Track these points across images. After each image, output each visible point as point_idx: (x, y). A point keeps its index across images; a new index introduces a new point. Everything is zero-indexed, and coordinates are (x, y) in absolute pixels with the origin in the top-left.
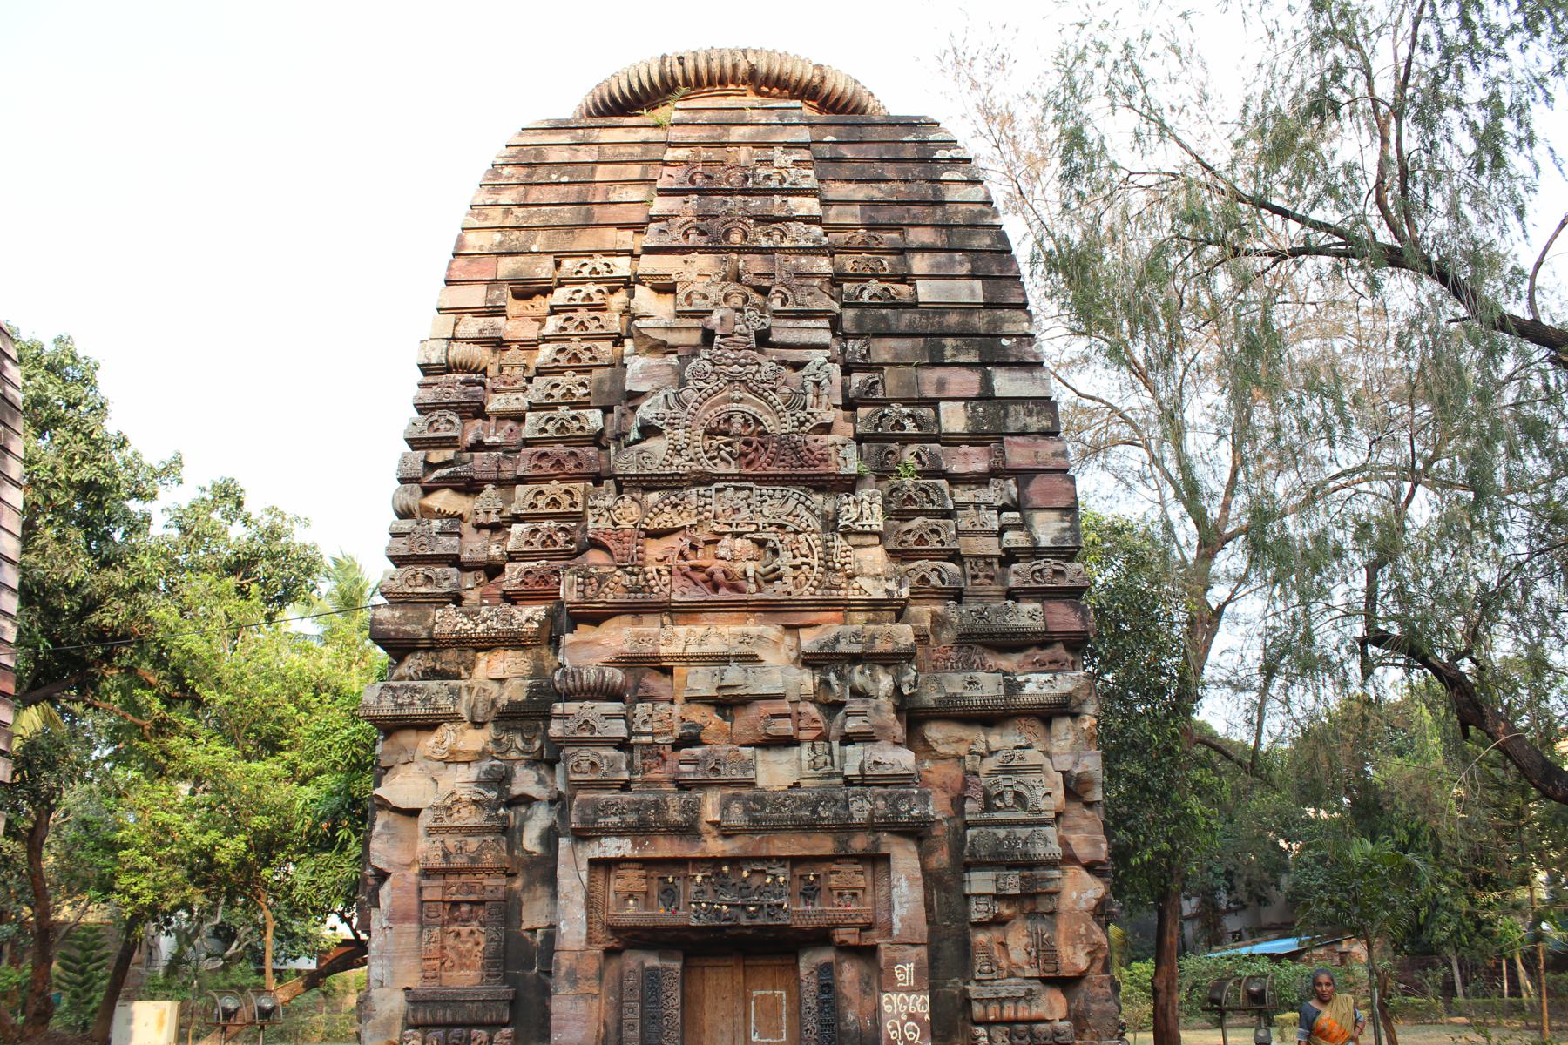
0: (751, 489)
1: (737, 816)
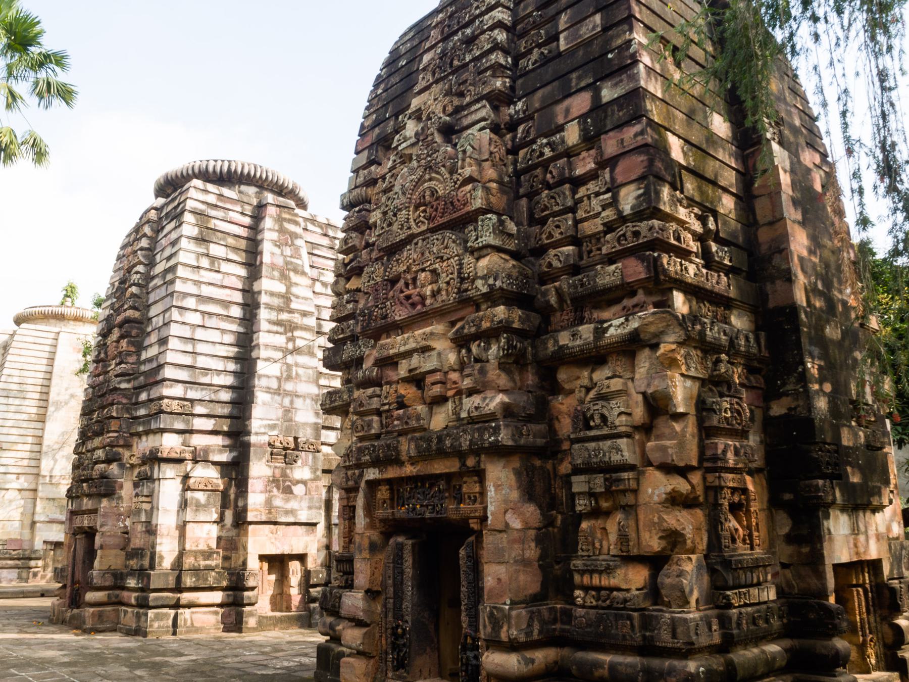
0: (428, 238)
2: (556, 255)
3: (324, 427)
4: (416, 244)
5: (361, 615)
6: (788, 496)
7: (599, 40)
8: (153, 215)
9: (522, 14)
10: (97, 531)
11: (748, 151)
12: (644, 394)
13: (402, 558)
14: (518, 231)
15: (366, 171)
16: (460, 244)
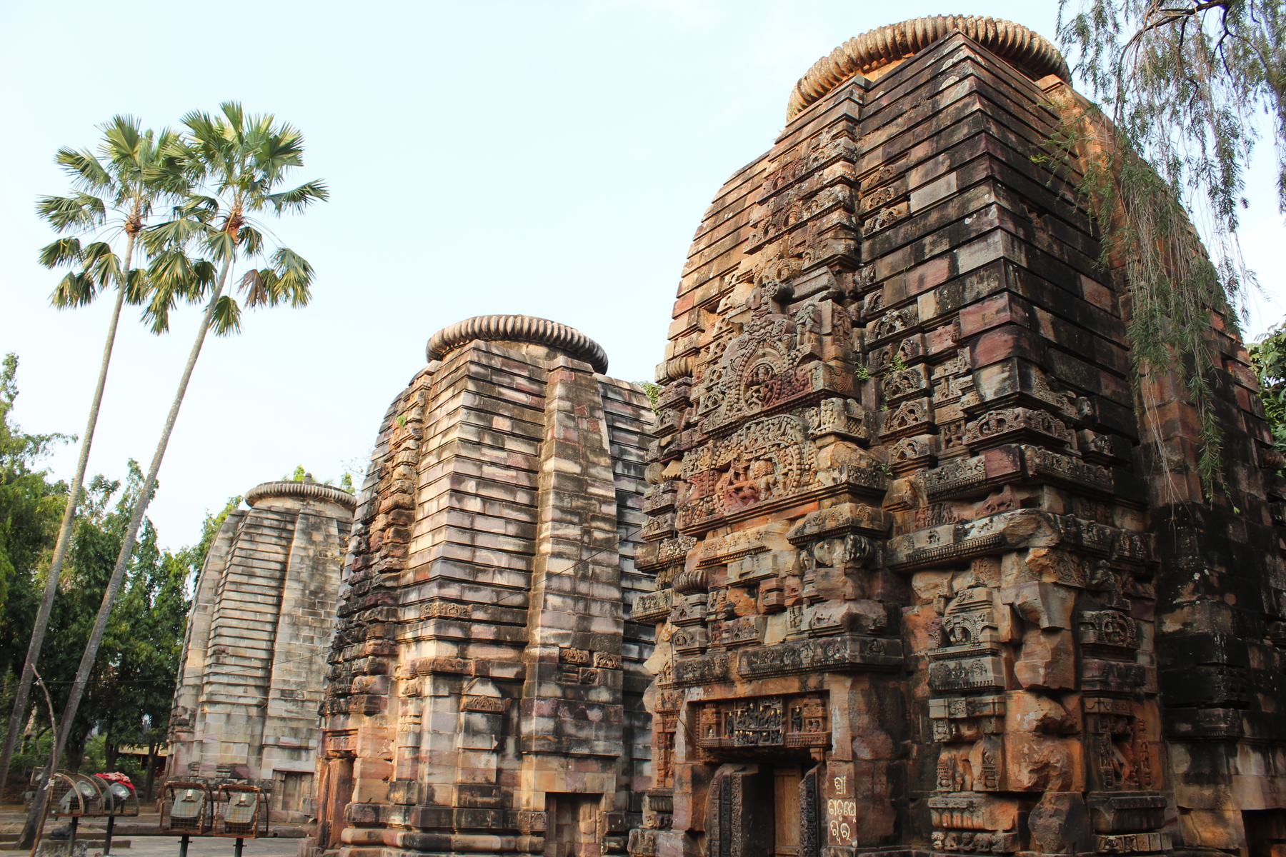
0: (762, 422)
1: (745, 670)
4: (749, 428)
6: (1185, 727)
8: (426, 380)
10: (356, 756)
12: (1011, 605)
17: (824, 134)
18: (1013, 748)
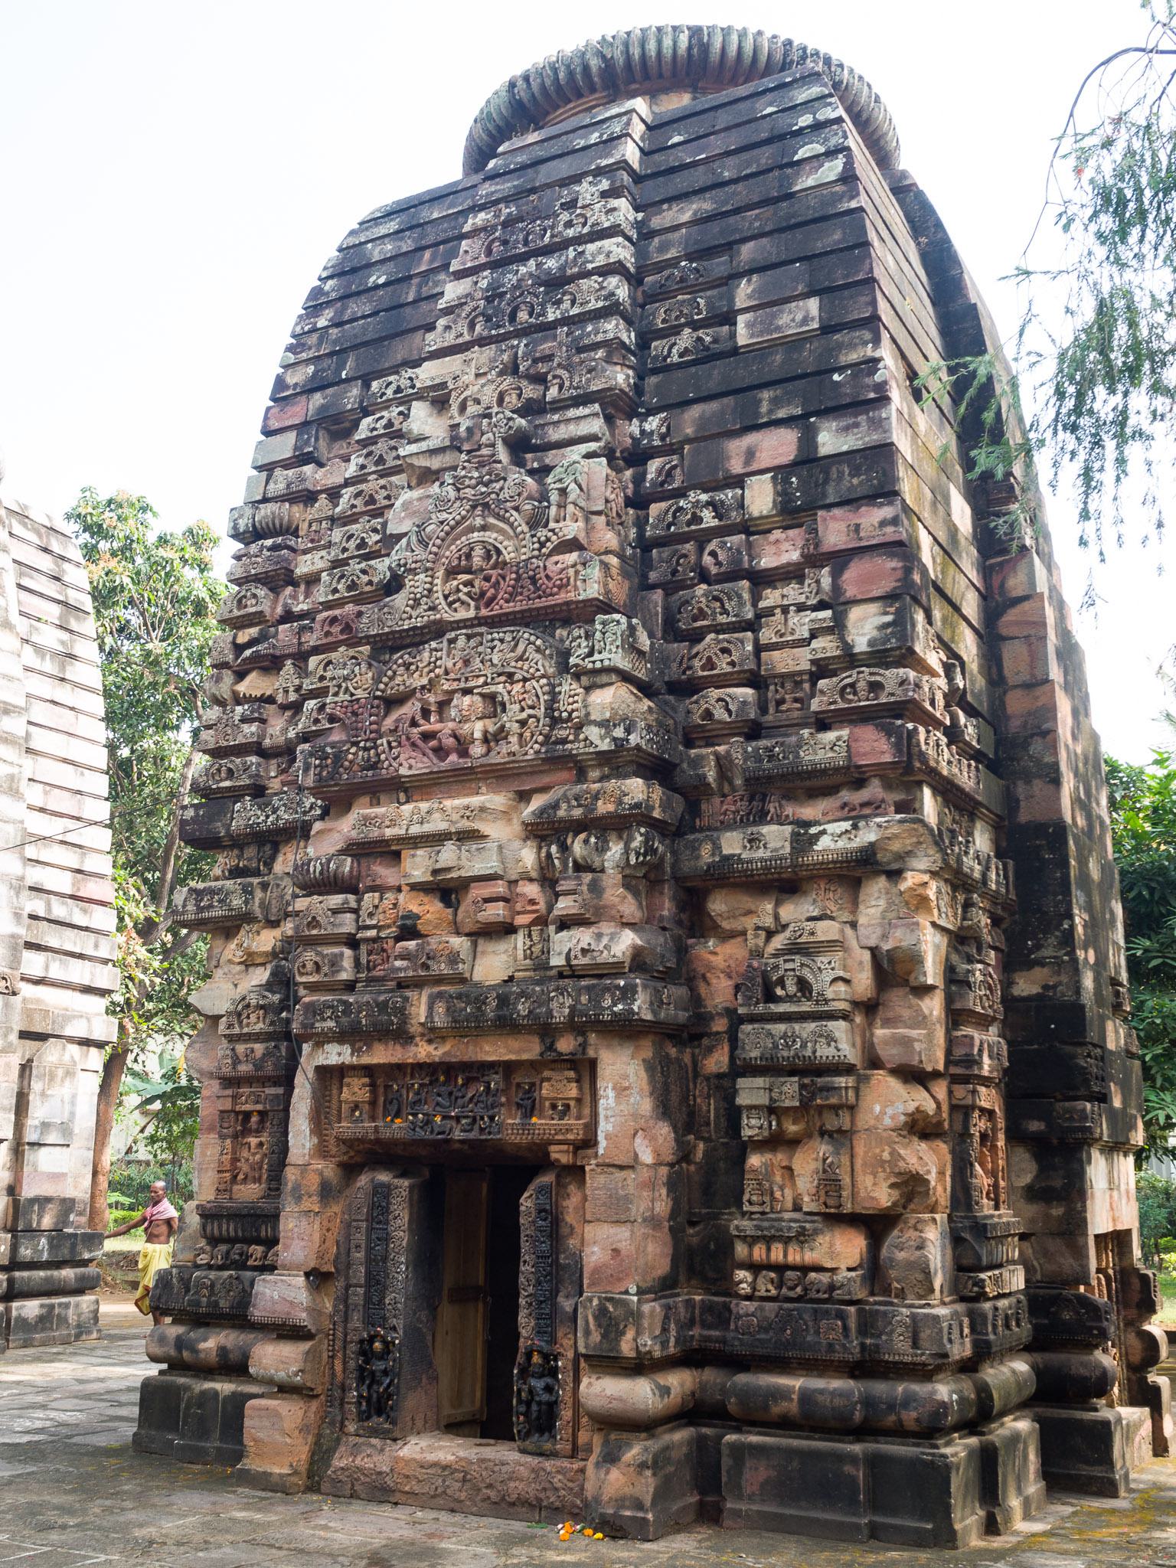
0: (481, 635)
1: (440, 1019)
2: (720, 700)
3: (30, 946)
4: (451, 641)
5: (302, 1317)
6: (1035, 1126)
7: (816, 344)
9: (657, 258)
11: (993, 561)
12: (874, 951)
13: (386, 1211)
14: (652, 645)
15: (290, 472)
16: (551, 656)
17: (585, 184)
18: (866, 1153)
